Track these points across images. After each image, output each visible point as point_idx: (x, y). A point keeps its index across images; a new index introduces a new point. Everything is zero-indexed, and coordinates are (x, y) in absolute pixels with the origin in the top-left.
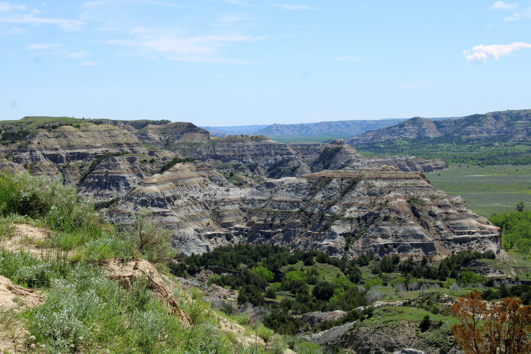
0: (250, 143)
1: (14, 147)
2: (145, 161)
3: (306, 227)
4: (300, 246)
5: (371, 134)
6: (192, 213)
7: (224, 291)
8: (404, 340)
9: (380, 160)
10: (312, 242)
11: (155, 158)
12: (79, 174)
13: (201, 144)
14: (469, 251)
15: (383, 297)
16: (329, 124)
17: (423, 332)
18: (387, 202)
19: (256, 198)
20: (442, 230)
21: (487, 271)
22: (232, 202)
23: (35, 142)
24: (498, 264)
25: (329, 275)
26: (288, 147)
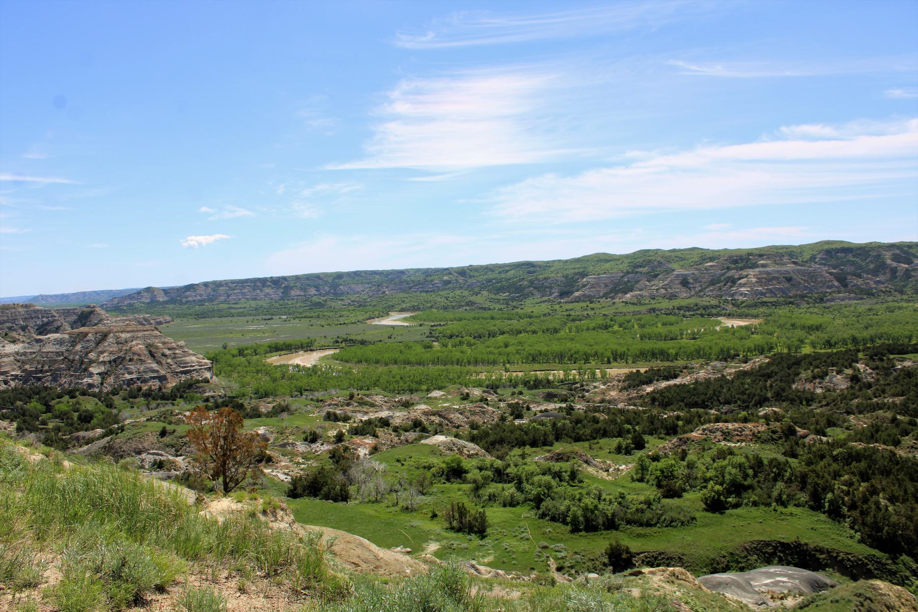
0: (20, 310)
21: (204, 392)
22: (7, 355)
25: (89, 404)
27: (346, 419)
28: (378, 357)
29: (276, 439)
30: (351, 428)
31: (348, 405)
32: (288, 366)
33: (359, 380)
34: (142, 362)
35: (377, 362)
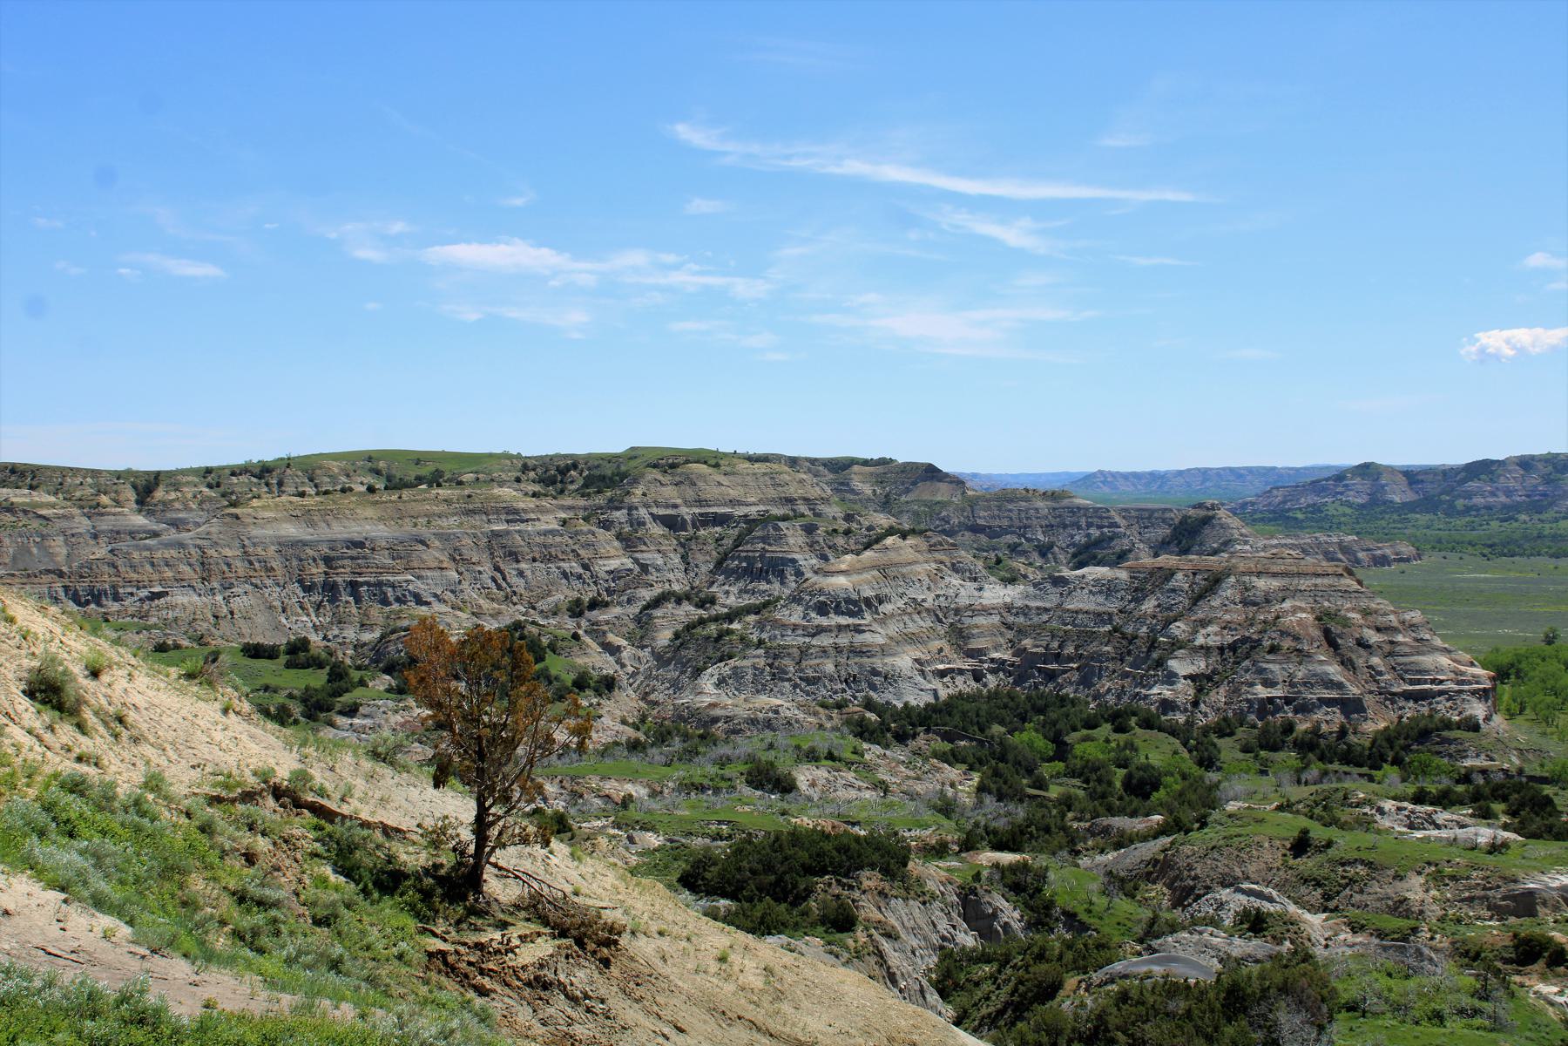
0: (1040, 504)
1: (600, 500)
2: (835, 531)
3: (1122, 660)
4: (1109, 697)
6: (912, 628)
7: (953, 773)
8: (1259, 871)
9: (1289, 541)
10: (1132, 690)
11: (854, 526)
14: (1431, 716)
15: (1250, 795)
16: (1204, 473)
17: (1295, 857)
18: (1278, 617)
19: (1033, 604)
20: (1380, 673)
22: (986, 611)
23: (639, 492)
24: (1484, 742)
25: (1157, 752)
26: (1113, 513)
34: (1302, 656)
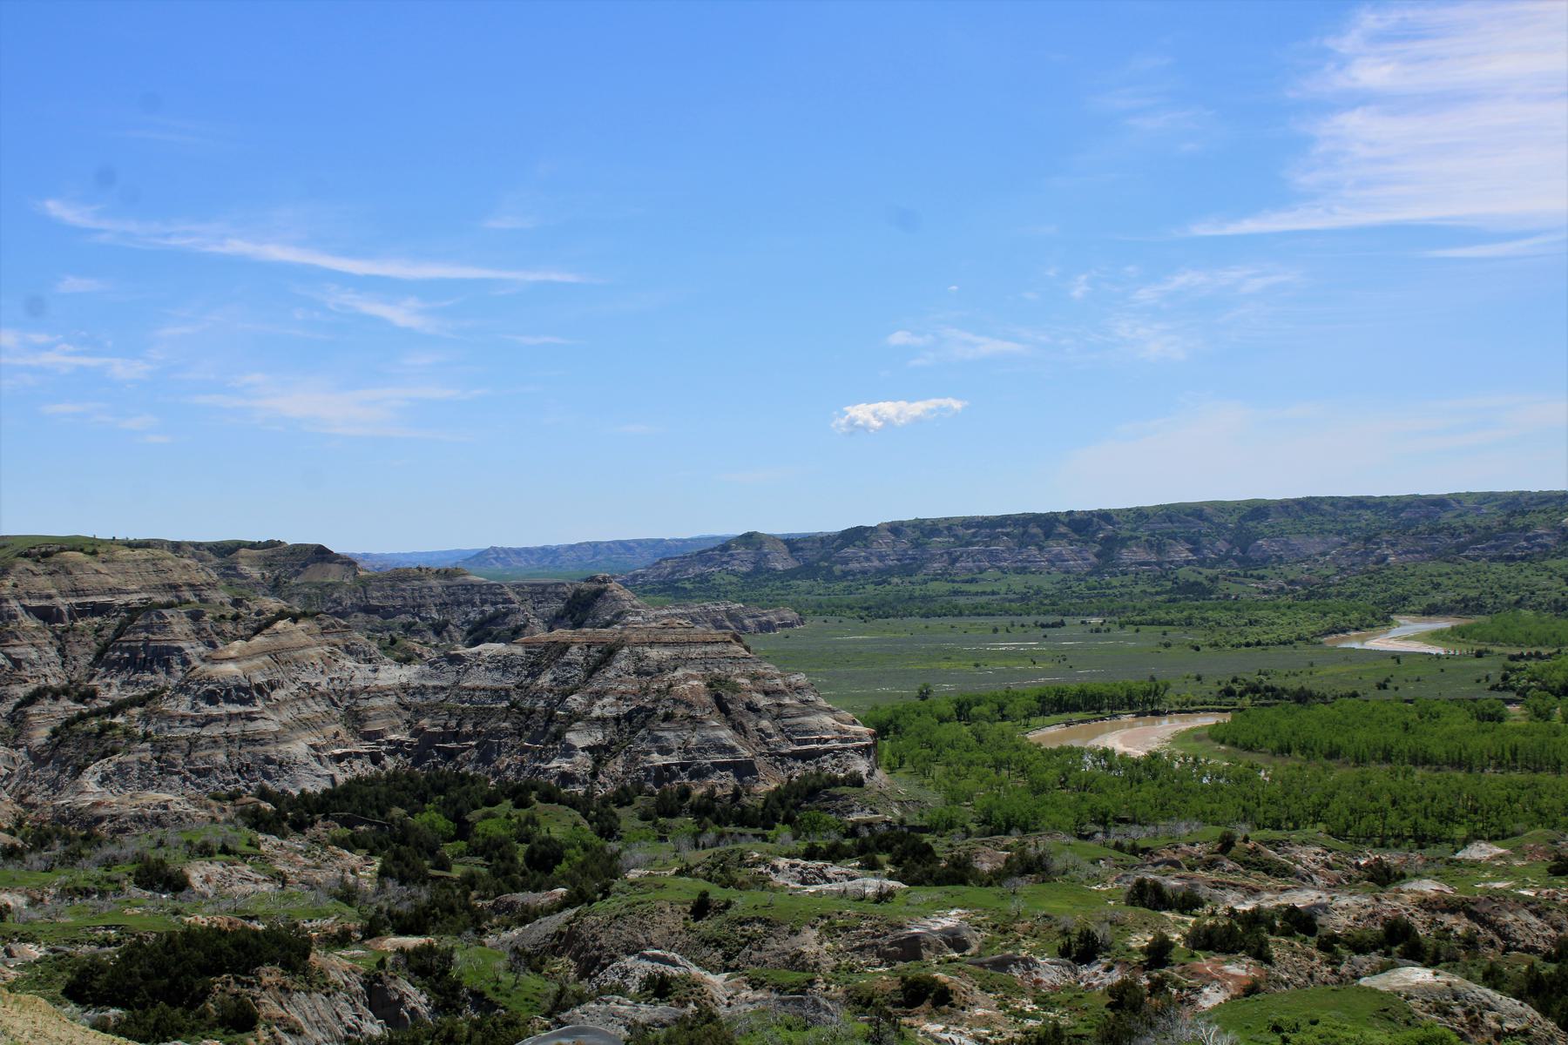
0: (434, 582)
2: (223, 617)
3: (520, 735)
4: (508, 773)
5: (670, 563)
6: (307, 713)
11: (243, 611)
12: (94, 645)
13: (342, 584)
14: (818, 775)
15: (651, 862)
18: (671, 686)
20: (770, 736)
21: (848, 809)
22: (382, 692)
24: (868, 796)
25: (558, 825)
26: (507, 589)
27: (1188, 903)
28: (1338, 740)
29: (987, 945)
30: (1196, 929)
31: (1210, 865)
32: (1081, 752)
33: (1272, 801)
34: (697, 723)
35: (1333, 754)
